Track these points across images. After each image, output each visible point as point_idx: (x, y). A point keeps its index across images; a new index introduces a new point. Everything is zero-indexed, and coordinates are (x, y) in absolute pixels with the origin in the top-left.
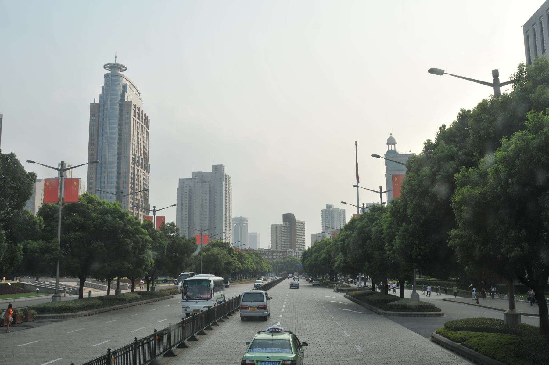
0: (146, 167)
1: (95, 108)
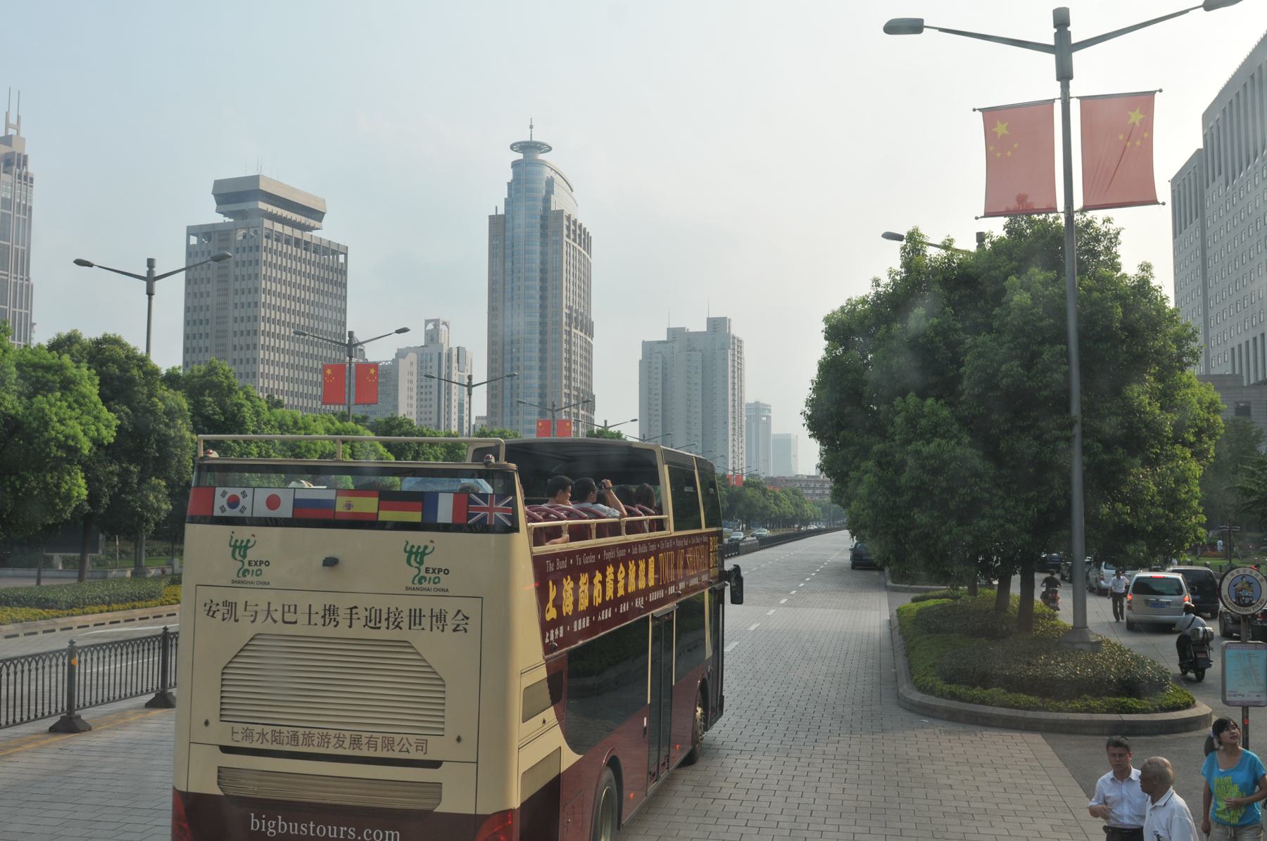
0: (588, 329)
1: (497, 224)
